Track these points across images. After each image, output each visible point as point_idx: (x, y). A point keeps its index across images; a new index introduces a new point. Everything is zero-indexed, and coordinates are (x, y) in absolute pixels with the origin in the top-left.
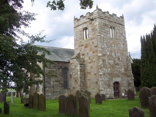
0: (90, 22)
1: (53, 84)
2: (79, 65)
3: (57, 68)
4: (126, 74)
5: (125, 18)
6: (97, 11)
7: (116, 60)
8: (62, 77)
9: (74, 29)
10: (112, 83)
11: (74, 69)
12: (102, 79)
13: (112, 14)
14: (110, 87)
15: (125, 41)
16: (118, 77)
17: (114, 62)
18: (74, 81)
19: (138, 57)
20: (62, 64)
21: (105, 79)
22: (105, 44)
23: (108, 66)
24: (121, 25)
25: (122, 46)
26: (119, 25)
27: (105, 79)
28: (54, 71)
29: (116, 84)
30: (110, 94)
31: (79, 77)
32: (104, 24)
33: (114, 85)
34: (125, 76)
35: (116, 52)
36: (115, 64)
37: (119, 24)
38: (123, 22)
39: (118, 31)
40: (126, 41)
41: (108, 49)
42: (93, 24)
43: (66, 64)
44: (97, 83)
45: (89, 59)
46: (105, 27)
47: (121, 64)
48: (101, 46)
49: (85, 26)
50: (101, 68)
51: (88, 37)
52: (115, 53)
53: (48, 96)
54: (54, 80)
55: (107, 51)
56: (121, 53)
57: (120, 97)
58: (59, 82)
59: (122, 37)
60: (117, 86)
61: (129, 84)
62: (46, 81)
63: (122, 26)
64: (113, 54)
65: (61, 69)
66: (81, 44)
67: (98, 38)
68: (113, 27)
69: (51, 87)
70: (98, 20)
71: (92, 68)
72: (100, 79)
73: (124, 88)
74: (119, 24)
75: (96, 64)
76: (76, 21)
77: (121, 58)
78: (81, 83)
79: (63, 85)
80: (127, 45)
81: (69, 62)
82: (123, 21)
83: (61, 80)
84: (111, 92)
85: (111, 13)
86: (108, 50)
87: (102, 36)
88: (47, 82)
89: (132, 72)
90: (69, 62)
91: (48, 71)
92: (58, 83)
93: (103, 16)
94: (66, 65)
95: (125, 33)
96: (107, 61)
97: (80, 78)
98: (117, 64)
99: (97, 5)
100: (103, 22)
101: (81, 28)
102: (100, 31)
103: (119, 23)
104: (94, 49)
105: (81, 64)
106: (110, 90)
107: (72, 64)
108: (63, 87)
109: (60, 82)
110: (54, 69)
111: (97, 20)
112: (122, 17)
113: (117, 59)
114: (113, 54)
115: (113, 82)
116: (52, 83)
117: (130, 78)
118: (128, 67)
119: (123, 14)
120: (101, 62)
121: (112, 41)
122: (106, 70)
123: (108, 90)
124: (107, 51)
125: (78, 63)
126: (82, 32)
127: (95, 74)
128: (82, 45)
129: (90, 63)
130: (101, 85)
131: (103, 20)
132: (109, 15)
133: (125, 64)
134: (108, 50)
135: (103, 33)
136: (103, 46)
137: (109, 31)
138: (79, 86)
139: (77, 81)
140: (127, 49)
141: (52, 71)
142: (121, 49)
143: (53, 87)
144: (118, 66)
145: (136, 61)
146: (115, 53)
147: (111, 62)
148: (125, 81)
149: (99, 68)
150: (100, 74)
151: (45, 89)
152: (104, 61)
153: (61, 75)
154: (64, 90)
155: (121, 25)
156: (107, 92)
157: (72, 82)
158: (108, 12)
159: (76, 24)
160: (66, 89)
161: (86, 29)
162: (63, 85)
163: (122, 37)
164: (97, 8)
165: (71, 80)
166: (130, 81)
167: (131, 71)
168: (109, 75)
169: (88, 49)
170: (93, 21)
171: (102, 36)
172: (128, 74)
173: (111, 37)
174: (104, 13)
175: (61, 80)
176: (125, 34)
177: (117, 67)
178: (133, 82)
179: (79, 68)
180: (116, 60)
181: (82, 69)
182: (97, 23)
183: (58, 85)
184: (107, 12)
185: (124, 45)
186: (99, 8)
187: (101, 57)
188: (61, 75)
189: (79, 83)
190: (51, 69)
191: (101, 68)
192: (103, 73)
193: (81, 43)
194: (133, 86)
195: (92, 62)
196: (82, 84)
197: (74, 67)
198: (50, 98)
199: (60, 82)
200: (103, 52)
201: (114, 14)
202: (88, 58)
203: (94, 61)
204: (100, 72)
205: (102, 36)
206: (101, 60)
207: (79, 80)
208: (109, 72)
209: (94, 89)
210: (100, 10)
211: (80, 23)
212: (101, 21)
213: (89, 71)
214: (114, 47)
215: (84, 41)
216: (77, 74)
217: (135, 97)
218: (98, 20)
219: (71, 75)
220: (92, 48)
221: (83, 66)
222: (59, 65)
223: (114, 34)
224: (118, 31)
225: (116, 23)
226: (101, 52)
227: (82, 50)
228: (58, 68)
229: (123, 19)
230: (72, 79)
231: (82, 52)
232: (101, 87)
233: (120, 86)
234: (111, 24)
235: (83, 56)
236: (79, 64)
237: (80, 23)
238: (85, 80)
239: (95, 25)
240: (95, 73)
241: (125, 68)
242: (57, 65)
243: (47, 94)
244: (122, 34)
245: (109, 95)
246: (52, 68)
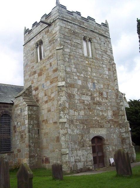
2: (27, 108)
4: (115, 122)
5: (109, 25)
7: (95, 95)
9: (24, 48)
10: (87, 139)
11: (19, 115)
12: (65, 131)
13: (86, 18)
14: (83, 146)
15: (112, 63)
16: (101, 127)
17: (91, 99)
18: (19, 137)
21: (73, 131)
22: (74, 66)
23: (80, 106)
24: (104, 36)
25: (107, 72)
26: (100, 36)
27: (73, 131)
30: (84, 162)
31: (27, 130)
32: (70, 30)
33: (92, 143)
34: (114, 125)
35: (96, 82)
36: (94, 103)
37: (100, 34)
38: (107, 33)
39: (97, 46)
41: (78, 74)
42: (50, 33)
43: (7, 107)
44: (58, 139)
45: (46, 95)
46: (74, 36)
47: (106, 103)
48: (64, 68)
49: (39, 38)
50: (63, 110)
51: (44, 55)
52: (94, 83)
55: (76, 78)
56: (104, 85)
57: (105, 165)
60: (98, 144)
61: (123, 140)
63: (106, 39)
64: (90, 85)
66: (34, 70)
67: (59, 54)
68: (88, 39)
70: (59, 23)
71: (49, 111)
72: (62, 132)
73: (114, 148)
74: (100, 34)
75: (55, 103)
76: (27, 33)
77: (105, 93)
78: (29, 141)
80: (115, 70)
81: (12, 104)
82: (107, 31)
84: (87, 157)
85: (85, 15)
87: (67, 50)
89: (126, 118)
90: (12, 104)
93: (68, 17)
94: (7, 109)
95: (111, 51)
96: (77, 97)
97: (29, 132)
98: (99, 103)
100: (69, 27)
101: (33, 43)
102: (62, 42)
103: (100, 33)
104: (53, 75)
105: (30, 105)
106: (85, 153)
107: (16, 106)
111: (58, 24)
113: (98, 93)
114: (90, 85)
117: (123, 130)
119: (106, 21)
120: (64, 98)
121: (87, 62)
122: (76, 113)
123: (80, 153)
124: (76, 78)
125: (25, 103)
126: (35, 50)
127: (55, 123)
128: (35, 73)
129: (46, 102)
130: (63, 143)
131: (69, 24)
132: (80, 17)
135: (70, 47)
136: (68, 69)
137: (81, 44)
138: (26, 147)
139: (24, 136)
140: (116, 77)
144: (99, 106)
146: (94, 83)
147: (87, 99)
149: (60, 109)
150: (61, 120)
152: (71, 96)
155: (104, 36)
156: (78, 158)
158: (79, 13)
160: (6, 153)
161: (41, 43)
163: (105, 57)
164: (57, 3)
165: (14, 136)
166: (124, 134)
167: (126, 116)
168: (83, 123)
169: (43, 77)
170: (51, 27)
171: (67, 50)
172: (120, 122)
173: (86, 54)
174: (71, 13)
177: (99, 108)
178: (129, 135)
179: (26, 113)
180: (95, 95)
181: (32, 114)
182: (56, 29)
184: (77, 12)
185: (109, 70)
186: (62, 2)
189: (27, 139)
191: (63, 110)
193: (34, 69)
194: (129, 144)
195: (51, 99)
196: (32, 143)
197: (19, 112)
202: (43, 94)
203: (53, 98)
204: (63, 117)
206: (63, 94)
207: (27, 134)
208: (81, 117)
209: (54, 151)
210: (64, 7)
211: (32, 35)
212: (64, 26)
213: (45, 118)
214: (92, 72)
215: (37, 64)
216: (24, 124)
217: (132, 165)
218: (59, 23)
219: (15, 127)
220: (50, 75)
221: (35, 108)
223: (92, 50)
224: (97, 46)
225: (93, 32)
227: (34, 81)
229: (106, 28)
230: (17, 134)
231: (35, 85)
232: (63, 147)
233: (105, 145)
234: (85, 33)
235: (36, 91)
236: (26, 105)
237: (32, 35)
238: (39, 135)
239: (54, 32)
240: (55, 119)
241: (113, 111)
244: (106, 52)
245: (83, 163)
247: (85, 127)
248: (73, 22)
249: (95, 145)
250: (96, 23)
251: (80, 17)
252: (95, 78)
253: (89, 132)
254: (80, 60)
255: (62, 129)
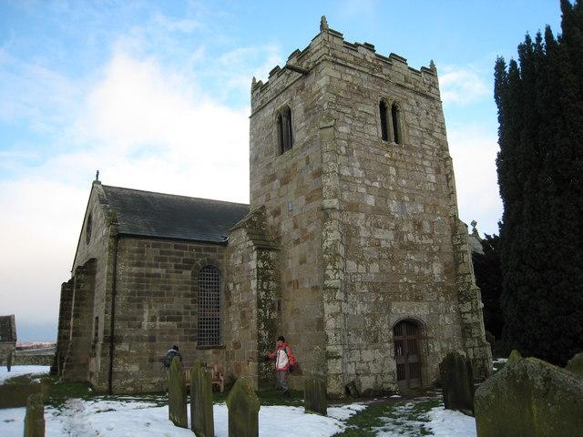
0: (299, 84)
1: (152, 330)
2: (255, 255)
3: (173, 264)
6: (325, 36)
7: (405, 229)
8: (193, 302)
10: (385, 326)
11: (238, 269)
14: (376, 341)
15: (445, 156)
16: (417, 299)
18: (238, 317)
19: (494, 231)
20: (198, 249)
22: (358, 164)
24: (427, 97)
25: (433, 178)
26: (418, 97)
27: (354, 306)
28: (158, 275)
29: (408, 333)
32: (350, 84)
33: (395, 334)
34: (445, 294)
35: (406, 198)
36: (402, 247)
38: (433, 90)
40: (449, 158)
41: (367, 182)
43: (214, 251)
46: (356, 98)
53: (127, 375)
54: (155, 310)
55: (363, 190)
58: (180, 319)
59: (429, 142)
61: (466, 330)
62: (119, 313)
65: (186, 268)
69: (140, 339)
73: (445, 345)
74: (417, 93)
77: (426, 225)
79: (192, 332)
80: (452, 172)
82: (434, 85)
83: (186, 313)
84: (383, 365)
86: (367, 186)
88: (123, 319)
89: (474, 281)
91: (130, 274)
92: (173, 325)
96: (363, 233)
97: (259, 305)
99: (323, 18)
100: (349, 78)
106: (379, 355)
108: (192, 339)
109: (184, 321)
110: (159, 270)
112: (431, 71)
114: (393, 206)
115: (394, 320)
116: (145, 324)
118: (460, 259)
121: (387, 155)
122: (362, 269)
123: (368, 355)
128: (273, 177)
129: (297, 242)
130: (331, 334)
131: (348, 71)
133: (447, 248)
134: (367, 186)
135: (349, 121)
136: (346, 172)
139: (248, 315)
141: (149, 275)
142: (428, 186)
143: (152, 339)
144: (413, 254)
145: (489, 242)
147: (386, 237)
148: (447, 319)
151: (112, 348)
153: (189, 292)
154: (199, 351)
155: (427, 97)
157: (232, 320)
158: (370, 47)
159: (258, 103)
160: (209, 348)
162: (192, 332)
163: (429, 142)
164: (322, 26)
167: (473, 276)
168: (376, 291)
169: (292, 186)
175: (186, 313)
176: (444, 134)
177: (413, 258)
178: (480, 319)
179: (253, 265)
181: (266, 268)
183: (172, 331)
184: (366, 44)
185: (438, 171)
187: (336, 215)
188: (189, 292)
190: (144, 270)
192: (345, 282)
195: (307, 237)
197: (239, 261)
198: (132, 385)
199: (184, 321)
200: (346, 195)
201: (394, 55)
202: (291, 225)
203: (312, 234)
204: (332, 276)
205: (340, 129)
210: (338, 35)
214: (398, 176)
216: (248, 289)
219: (228, 294)
221: (272, 255)
222: (182, 254)
225: (404, 88)
226: (335, 191)
227: (272, 196)
228: (176, 267)
230: (233, 308)
239: (314, 90)
241: (446, 265)
242: (170, 253)
243: (121, 370)
244: (430, 133)
245: (374, 377)
246: (150, 265)
247: (381, 299)
248: (357, 68)
249: (400, 338)
250: (409, 68)
251: (373, 55)
252: (405, 191)
253: (389, 311)
254: (372, 150)
255: (328, 302)
